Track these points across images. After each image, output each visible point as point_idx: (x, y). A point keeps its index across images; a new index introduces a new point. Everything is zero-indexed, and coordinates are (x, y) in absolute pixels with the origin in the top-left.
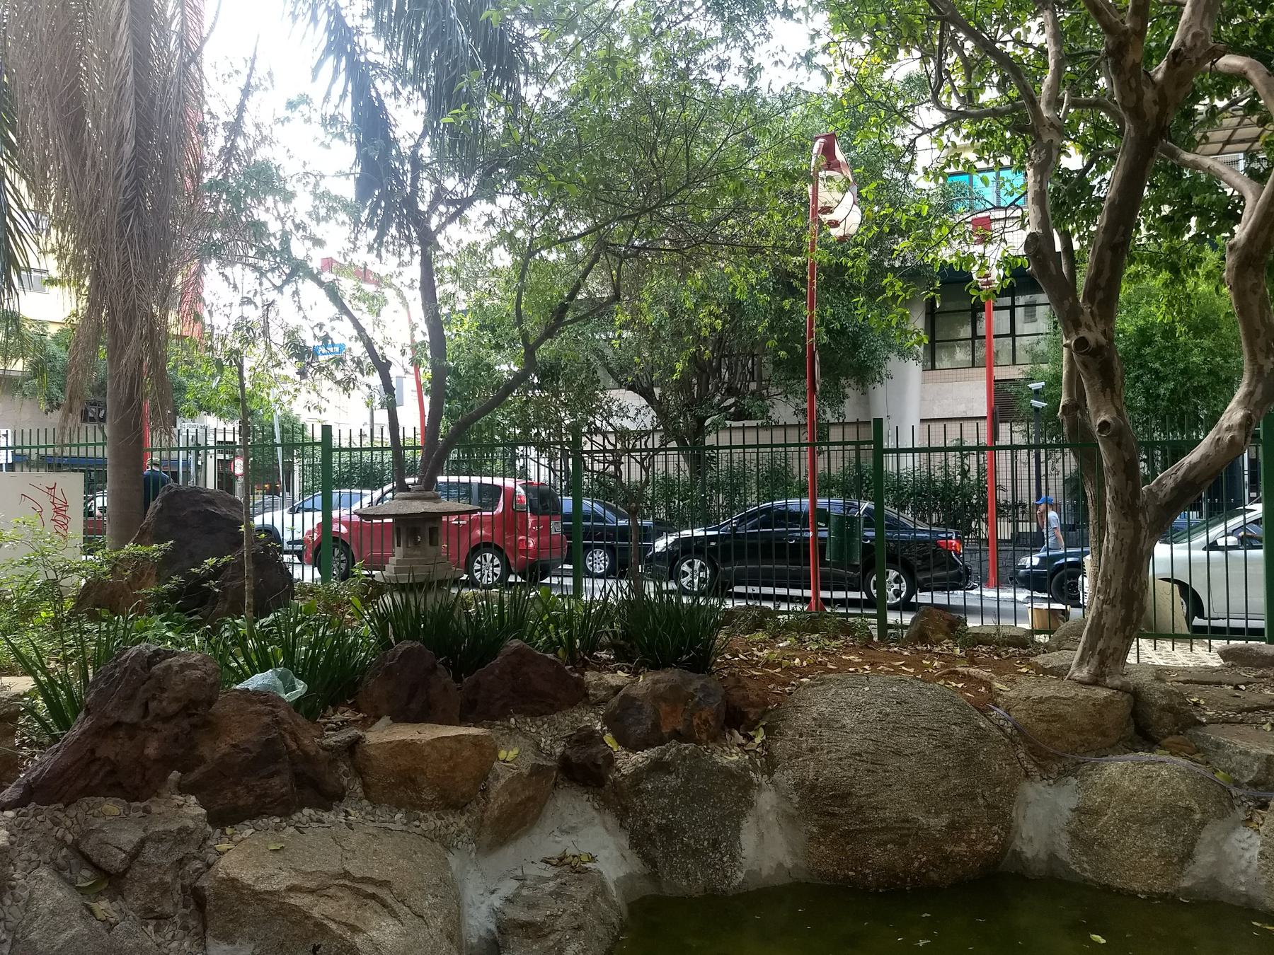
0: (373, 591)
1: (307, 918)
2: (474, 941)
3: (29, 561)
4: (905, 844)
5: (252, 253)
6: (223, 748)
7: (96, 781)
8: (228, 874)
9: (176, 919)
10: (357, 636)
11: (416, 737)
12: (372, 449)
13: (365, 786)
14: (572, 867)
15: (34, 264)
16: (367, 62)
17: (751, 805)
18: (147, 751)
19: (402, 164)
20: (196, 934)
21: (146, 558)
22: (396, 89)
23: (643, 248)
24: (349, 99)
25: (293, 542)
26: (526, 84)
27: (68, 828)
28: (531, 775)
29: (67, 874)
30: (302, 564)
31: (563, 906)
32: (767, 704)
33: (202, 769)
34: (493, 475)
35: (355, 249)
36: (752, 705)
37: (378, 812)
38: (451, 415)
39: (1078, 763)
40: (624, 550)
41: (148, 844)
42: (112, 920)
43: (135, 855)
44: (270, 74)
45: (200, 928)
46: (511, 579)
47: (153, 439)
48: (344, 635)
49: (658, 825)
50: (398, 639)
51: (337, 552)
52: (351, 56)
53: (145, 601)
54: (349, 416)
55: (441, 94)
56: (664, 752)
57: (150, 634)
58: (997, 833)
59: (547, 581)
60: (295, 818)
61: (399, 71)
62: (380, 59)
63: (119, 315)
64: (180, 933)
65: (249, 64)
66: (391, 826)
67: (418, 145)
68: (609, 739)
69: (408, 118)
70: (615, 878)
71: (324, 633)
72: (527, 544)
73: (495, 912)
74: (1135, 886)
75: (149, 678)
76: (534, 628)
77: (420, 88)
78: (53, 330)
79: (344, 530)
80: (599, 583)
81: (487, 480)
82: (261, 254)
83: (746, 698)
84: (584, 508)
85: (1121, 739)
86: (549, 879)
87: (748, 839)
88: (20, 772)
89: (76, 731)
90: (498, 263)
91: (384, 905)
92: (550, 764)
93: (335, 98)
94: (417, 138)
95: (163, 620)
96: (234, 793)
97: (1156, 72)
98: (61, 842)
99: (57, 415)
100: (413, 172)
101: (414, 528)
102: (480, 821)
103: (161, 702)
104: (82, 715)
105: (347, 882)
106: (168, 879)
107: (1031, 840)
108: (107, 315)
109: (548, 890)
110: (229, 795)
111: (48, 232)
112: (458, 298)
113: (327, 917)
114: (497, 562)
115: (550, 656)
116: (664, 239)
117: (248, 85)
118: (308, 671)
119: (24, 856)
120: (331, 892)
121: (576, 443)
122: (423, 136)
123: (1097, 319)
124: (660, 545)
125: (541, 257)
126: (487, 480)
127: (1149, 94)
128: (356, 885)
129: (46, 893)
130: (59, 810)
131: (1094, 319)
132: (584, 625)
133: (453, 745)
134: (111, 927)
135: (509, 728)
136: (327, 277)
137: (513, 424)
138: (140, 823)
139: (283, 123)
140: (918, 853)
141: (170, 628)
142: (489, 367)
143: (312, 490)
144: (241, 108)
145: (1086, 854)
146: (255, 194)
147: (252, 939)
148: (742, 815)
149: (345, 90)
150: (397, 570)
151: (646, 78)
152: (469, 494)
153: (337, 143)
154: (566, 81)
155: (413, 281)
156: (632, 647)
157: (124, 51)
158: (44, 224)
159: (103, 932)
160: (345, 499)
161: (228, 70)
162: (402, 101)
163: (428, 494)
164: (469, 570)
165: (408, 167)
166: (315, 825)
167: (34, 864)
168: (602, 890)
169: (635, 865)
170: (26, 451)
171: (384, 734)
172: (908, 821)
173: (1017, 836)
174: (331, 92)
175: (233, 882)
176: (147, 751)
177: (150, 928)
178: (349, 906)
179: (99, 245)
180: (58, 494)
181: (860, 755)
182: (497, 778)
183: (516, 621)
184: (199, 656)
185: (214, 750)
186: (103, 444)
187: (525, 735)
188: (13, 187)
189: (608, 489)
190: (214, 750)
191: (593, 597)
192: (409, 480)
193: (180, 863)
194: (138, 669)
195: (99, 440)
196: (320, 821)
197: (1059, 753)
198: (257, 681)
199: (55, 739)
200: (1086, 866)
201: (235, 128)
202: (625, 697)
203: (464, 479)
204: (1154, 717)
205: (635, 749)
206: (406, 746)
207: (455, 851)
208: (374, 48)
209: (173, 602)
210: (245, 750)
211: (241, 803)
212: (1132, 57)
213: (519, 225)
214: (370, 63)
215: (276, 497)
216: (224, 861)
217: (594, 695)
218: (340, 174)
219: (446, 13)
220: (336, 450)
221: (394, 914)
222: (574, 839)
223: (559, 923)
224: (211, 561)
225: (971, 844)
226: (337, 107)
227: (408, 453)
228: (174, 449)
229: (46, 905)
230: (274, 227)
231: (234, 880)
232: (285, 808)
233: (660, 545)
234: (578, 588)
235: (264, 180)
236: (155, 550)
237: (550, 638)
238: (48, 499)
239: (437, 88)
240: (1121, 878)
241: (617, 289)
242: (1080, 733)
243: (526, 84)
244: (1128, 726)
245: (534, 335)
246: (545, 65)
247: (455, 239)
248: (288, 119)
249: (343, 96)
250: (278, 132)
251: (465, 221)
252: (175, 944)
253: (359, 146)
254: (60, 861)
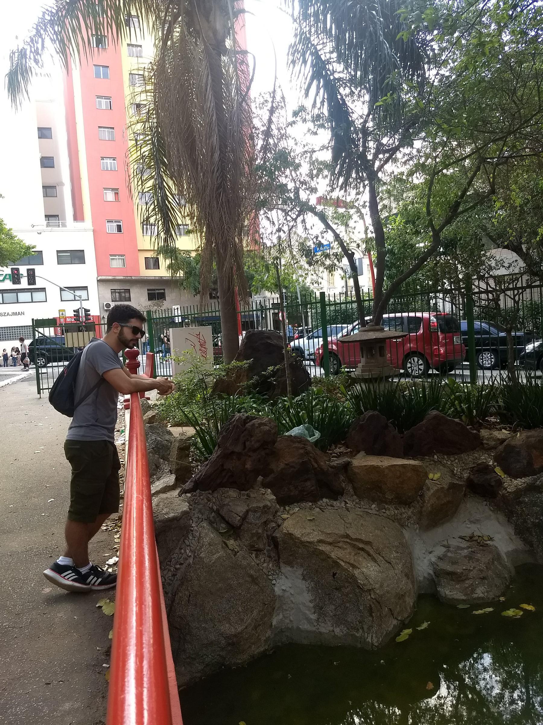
0: (351, 382)
1: (329, 557)
2: (421, 579)
3: (191, 371)
5: (280, 203)
6: (282, 466)
7: (225, 480)
8: (288, 531)
9: (265, 552)
10: (344, 407)
11: (380, 464)
12: (346, 303)
13: (354, 488)
14: (478, 543)
15: (180, 222)
16: (335, 79)
18: (246, 466)
19: (357, 135)
20: (275, 560)
21: (241, 368)
22: (352, 91)
23: (510, 157)
24: (326, 104)
25: (310, 355)
26: (429, 70)
27: (214, 503)
28: (449, 489)
29: (215, 525)
30: (315, 366)
31: (474, 565)
33: (272, 475)
34: (415, 311)
35: (333, 190)
37: (362, 503)
38: (390, 277)
40: (505, 352)
41: (250, 513)
42: (236, 550)
43: (244, 518)
44: (283, 98)
45: (277, 558)
46: (430, 372)
47: (241, 307)
48: (338, 407)
50: (366, 409)
51: (332, 360)
52: (326, 78)
53: (243, 389)
54: (332, 285)
55: (377, 88)
56: (536, 480)
57: (245, 405)
59: (453, 372)
60: (319, 503)
61: (353, 81)
62: (341, 75)
63: (220, 246)
64: (267, 559)
65: (272, 95)
66: (370, 511)
67: (366, 122)
68: (498, 470)
69: (359, 108)
70: (505, 550)
71: (327, 405)
72: (439, 351)
73: (432, 564)
75: (245, 430)
76: (446, 403)
77: (365, 87)
78: (193, 254)
79: (334, 347)
80: (488, 373)
81: (412, 314)
82: (285, 202)
84: (476, 326)
86: (464, 548)
88: (193, 474)
89: (214, 456)
90: (416, 181)
91: (369, 555)
92: (460, 483)
93: (318, 105)
94: (364, 117)
95: (251, 398)
98: (211, 509)
99: (198, 297)
100: (363, 138)
101: (371, 348)
102: (421, 512)
103: (251, 442)
104: (216, 448)
105: (348, 540)
106: (260, 531)
108: (215, 246)
109: (463, 554)
110: (286, 489)
111: (185, 206)
112: (391, 206)
113: (339, 558)
114: (421, 362)
115: (457, 420)
116: (525, 148)
117: (272, 107)
118: (320, 426)
119: (196, 515)
120: (340, 544)
121: (469, 288)
122: (368, 115)
124: (530, 347)
125: (443, 174)
126: (412, 314)
128: (353, 542)
129: (206, 534)
130: (209, 493)
132: (478, 401)
134: (236, 553)
135: (433, 461)
136: (319, 208)
137: (428, 278)
138: (246, 502)
139: (292, 126)
141: (254, 402)
142: (412, 246)
143: (317, 327)
144: (270, 121)
146: (279, 169)
147: (302, 566)
149: (324, 98)
150: (363, 371)
151: (507, 48)
152: (402, 323)
153: (321, 131)
154: (454, 63)
155: (365, 202)
156: (512, 415)
157: (210, 104)
158: (183, 202)
159: (232, 556)
160: (334, 331)
161: (262, 100)
162: (355, 98)
163: (377, 327)
164: (404, 367)
165: (360, 135)
166: (330, 508)
167: (201, 520)
168: (498, 557)
169: (518, 544)
170: (251, 313)
171: (362, 461)
174: (316, 100)
175: (290, 535)
176: (246, 466)
177: (253, 555)
178: (350, 553)
179: (208, 210)
180: (201, 338)
182: (428, 489)
183: (434, 399)
184: (267, 419)
185: (278, 466)
186: (219, 311)
187: (444, 466)
188: (168, 185)
189: (492, 313)
190: (278, 466)
191: (484, 382)
192: (367, 318)
193: (265, 523)
194: (240, 425)
195: (217, 309)
196: (332, 506)
198: (296, 431)
199: (206, 459)
201: (268, 134)
202: (508, 446)
203: (398, 315)
205: (516, 477)
206: (373, 468)
207: (407, 528)
208: (338, 70)
209: (255, 389)
210: (292, 467)
211: (292, 494)
213: (427, 156)
214: (336, 79)
216: (286, 524)
217: (487, 444)
218: (323, 148)
219: (377, 38)
220: (327, 305)
221: (375, 561)
222: (479, 526)
223: (471, 575)
224: (271, 368)
226: (319, 109)
227: (367, 303)
228: (251, 311)
229: (206, 540)
230: (291, 186)
231: (291, 534)
232: (314, 498)
233: (530, 347)
234: (474, 377)
235: (284, 160)
236: (245, 363)
237: (456, 409)
238: (197, 340)
239: (375, 85)
241: (492, 185)
243: (429, 70)
245: (437, 223)
246: (440, 55)
247: (389, 171)
248: (294, 122)
249: (322, 102)
250: (290, 131)
251: (395, 160)
252: (265, 565)
253: (333, 129)
254: (211, 518)
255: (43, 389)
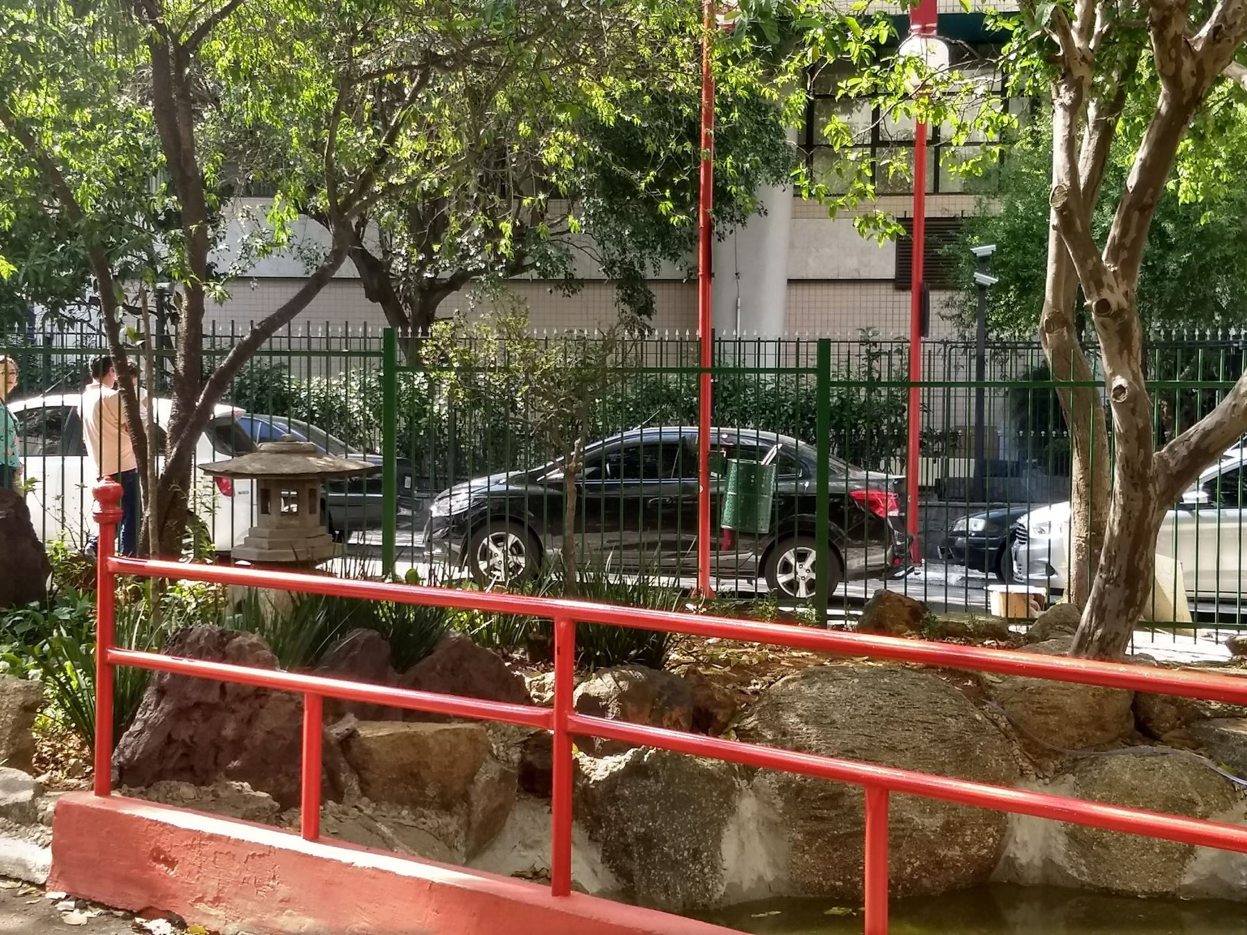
4: (899, 846)
17: (732, 811)
18: (224, 733)
28: (500, 780)
32: (735, 705)
36: (719, 705)
39: (1076, 760)
49: (636, 834)
58: (992, 836)
74: (1135, 886)
83: (711, 698)
85: (1120, 736)
87: (729, 849)
96: (277, 780)
97: (1196, 41)
107: (1025, 844)
123: (1120, 280)
127: (1188, 65)
131: (1116, 279)
133: (452, 738)
140: (910, 856)
145: (1084, 856)
148: (720, 824)
172: (902, 821)
173: (1012, 840)
176: (224, 733)
181: (853, 752)
197: (1056, 748)
200: (1084, 869)
204: (1156, 709)
205: (600, 755)
212: (1174, 29)
215: (72, 462)
225: (965, 846)
240: (1120, 879)
242: (1079, 725)
244: (1128, 720)
255: (967, 384)
